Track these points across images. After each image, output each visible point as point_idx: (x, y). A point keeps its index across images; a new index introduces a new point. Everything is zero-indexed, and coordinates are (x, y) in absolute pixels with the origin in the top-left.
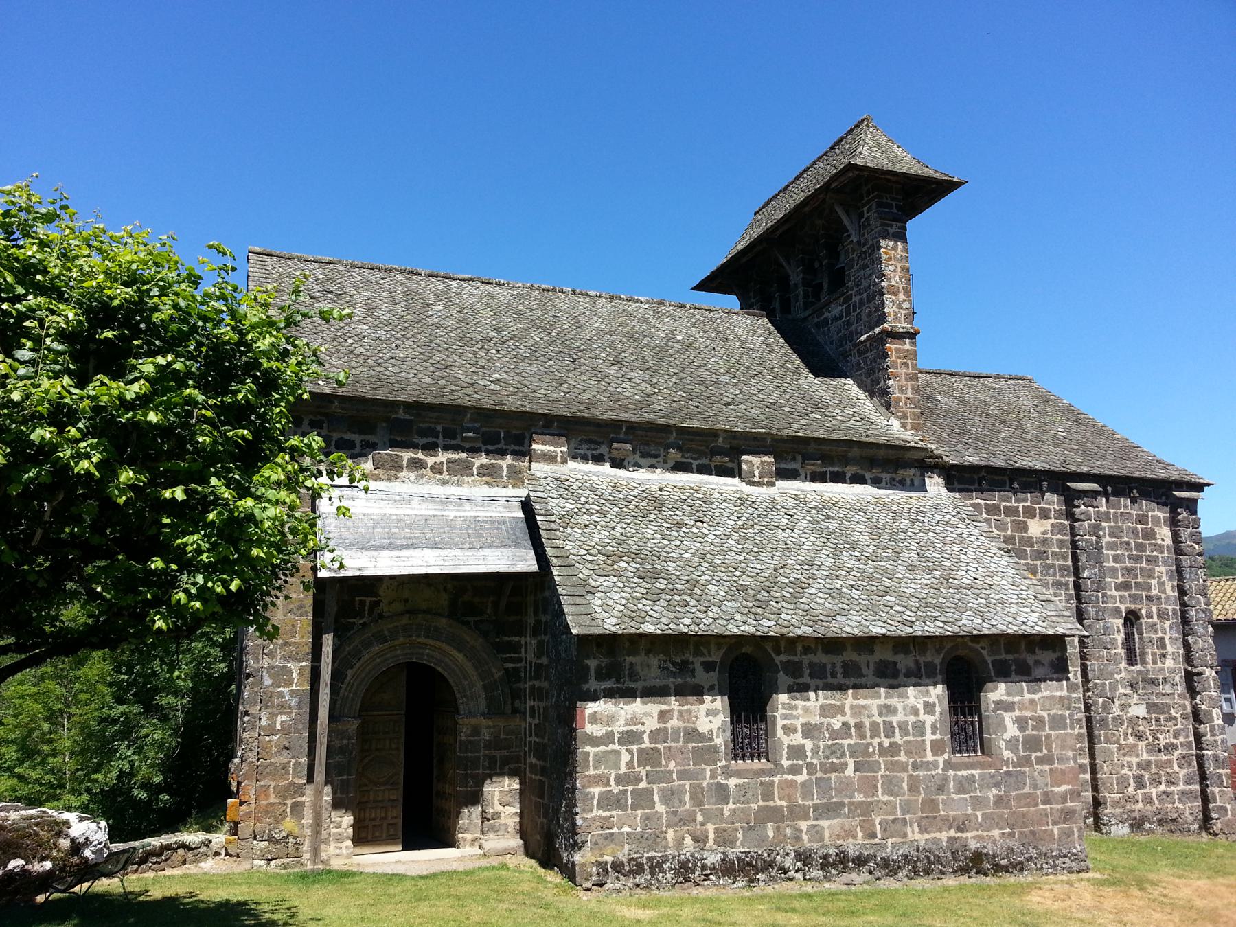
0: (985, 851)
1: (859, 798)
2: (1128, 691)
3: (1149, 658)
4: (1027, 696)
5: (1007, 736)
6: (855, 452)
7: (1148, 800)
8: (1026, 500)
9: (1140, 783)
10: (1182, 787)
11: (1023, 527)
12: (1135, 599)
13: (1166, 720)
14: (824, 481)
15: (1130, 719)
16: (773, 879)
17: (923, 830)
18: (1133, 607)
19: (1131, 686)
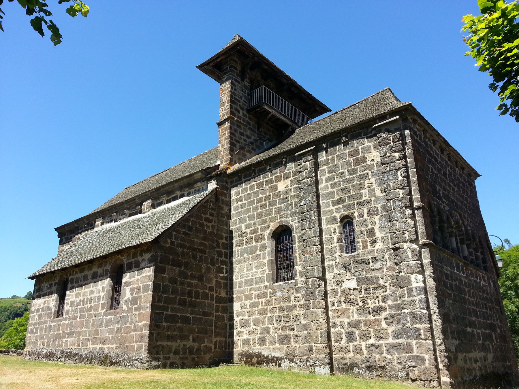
0: (109, 355)
1: (78, 329)
2: (343, 271)
3: (360, 245)
4: (137, 277)
5: (126, 298)
6: (176, 185)
7: (358, 350)
8: (276, 173)
9: (350, 337)
10: (391, 340)
11: (275, 188)
12: (348, 207)
13: (375, 288)
14: (170, 202)
15: (344, 291)
16: (54, 360)
17: (93, 344)
18: (346, 213)
19: (345, 267)
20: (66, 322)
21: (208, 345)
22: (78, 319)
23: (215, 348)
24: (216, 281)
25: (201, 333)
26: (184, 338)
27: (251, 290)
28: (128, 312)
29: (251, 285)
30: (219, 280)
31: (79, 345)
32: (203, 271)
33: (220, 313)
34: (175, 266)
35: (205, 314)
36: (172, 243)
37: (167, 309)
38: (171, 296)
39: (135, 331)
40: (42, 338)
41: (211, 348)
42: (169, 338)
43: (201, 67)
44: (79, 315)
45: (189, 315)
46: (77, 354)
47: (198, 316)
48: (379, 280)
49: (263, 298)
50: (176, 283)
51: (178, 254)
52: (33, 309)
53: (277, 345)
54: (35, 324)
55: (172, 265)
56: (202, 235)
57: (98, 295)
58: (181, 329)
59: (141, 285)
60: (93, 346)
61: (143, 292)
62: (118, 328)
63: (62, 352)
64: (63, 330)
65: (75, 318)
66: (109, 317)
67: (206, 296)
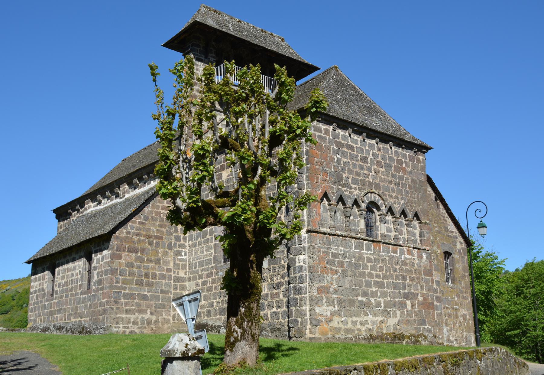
1: (65, 307)
20: (56, 301)
21: (165, 317)
22: (64, 298)
23: (174, 320)
24: (175, 263)
25: (159, 308)
26: (141, 311)
27: (202, 270)
28: (96, 291)
29: (203, 266)
30: (177, 262)
31: (65, 320)
32: (160, 255)
33: (178, 291)
34: (132, 252)
35: (162, 292)
36: (128, 233)
37: (125, 289)
38: (128, 278)
39: (100, 306)
40: (40, 316)
41: (169, 320)
42: (127, 312)
43: (164, 45)
44: (64, 294)
45: (146, 293)
46: (64, 327)
47: (156, 294)
48: (281, 261)
49: (210, 277)
50: (132, 267)
51: (134, 242)
52: (32, 290)
53: (218, 316)
54: (34, 304)
55: (128, 252)
56: (158, 223)
57: (76, 277)
58: (138, 305)
59: (103, 269)
60: (75, 320)
61: (105, 276)
62: (90, 305)
63: (54, 326)
64: (54, 308)
65: (62, 297)
66: (84, 296)
67: (163, 277)
